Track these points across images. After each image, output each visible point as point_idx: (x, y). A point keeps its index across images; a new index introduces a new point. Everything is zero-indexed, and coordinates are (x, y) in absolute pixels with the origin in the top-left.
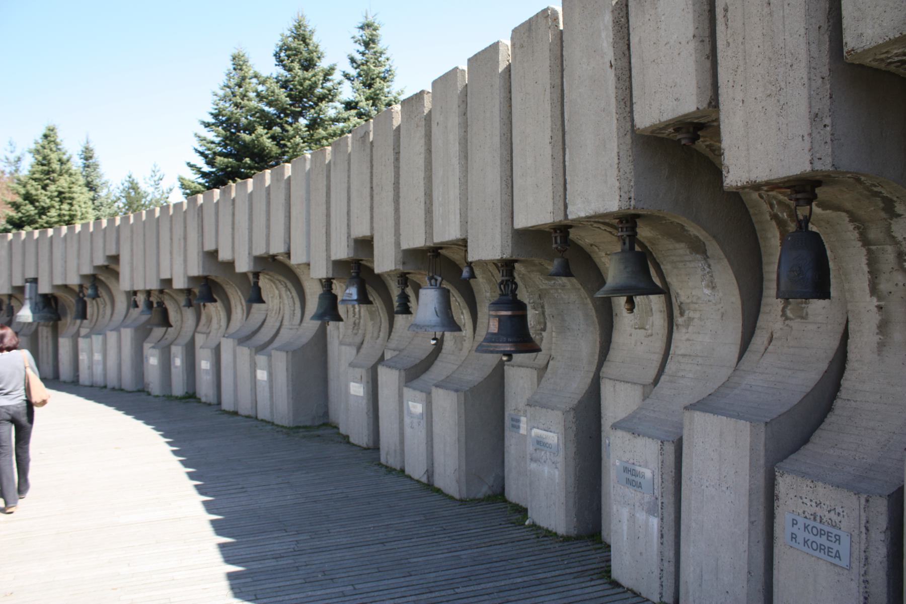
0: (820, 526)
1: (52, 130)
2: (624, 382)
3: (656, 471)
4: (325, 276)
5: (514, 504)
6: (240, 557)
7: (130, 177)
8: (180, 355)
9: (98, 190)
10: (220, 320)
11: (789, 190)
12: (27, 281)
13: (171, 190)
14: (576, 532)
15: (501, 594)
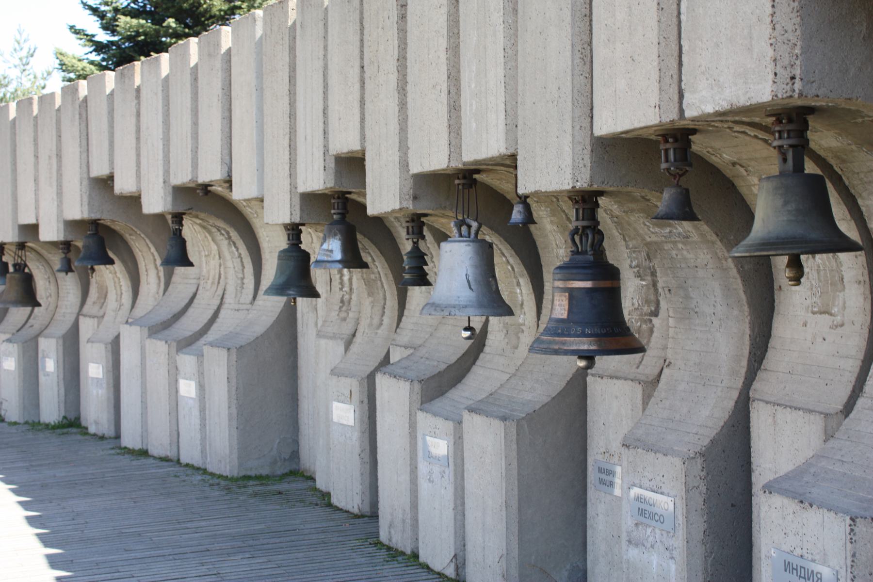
2: (791, 407)
3: (843, 572)
8: (53, 354)
10: (122, 294)
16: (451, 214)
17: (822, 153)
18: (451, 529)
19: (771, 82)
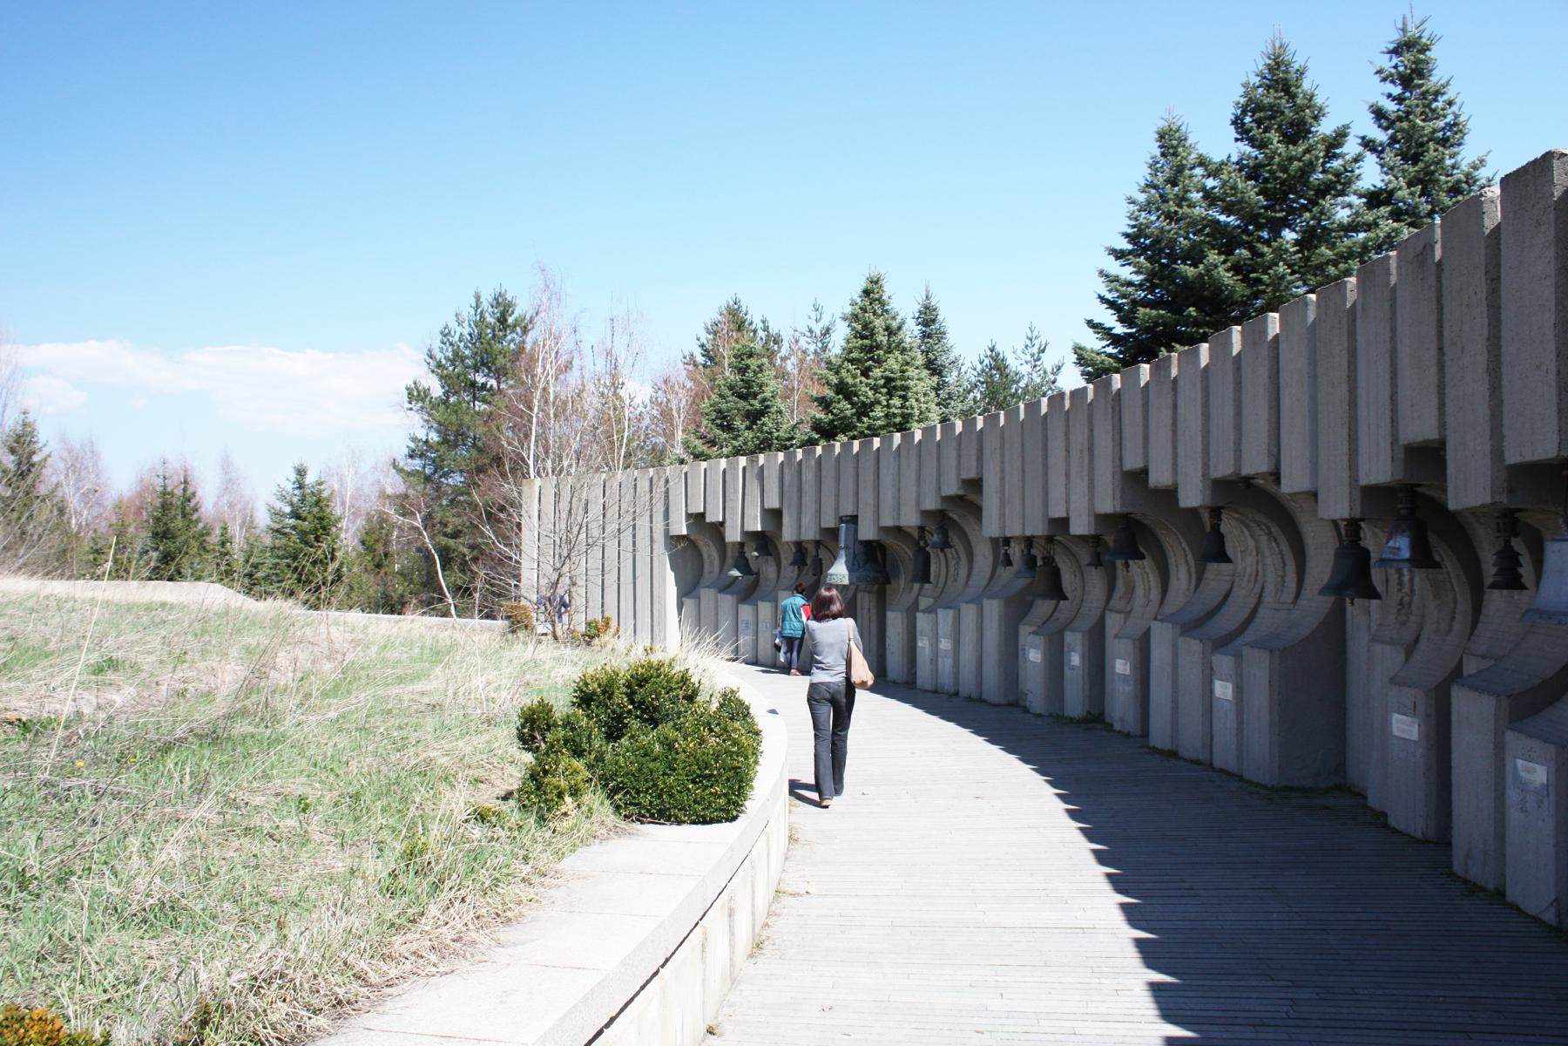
1: (876, 282)
4: (1346, 515)
6: (1189, 1013)
7: (992, 351)
8: (1079, 648)
9: (944, 373)
10: (1150, 589)
12: (841, 520)
13: (1059, 368)
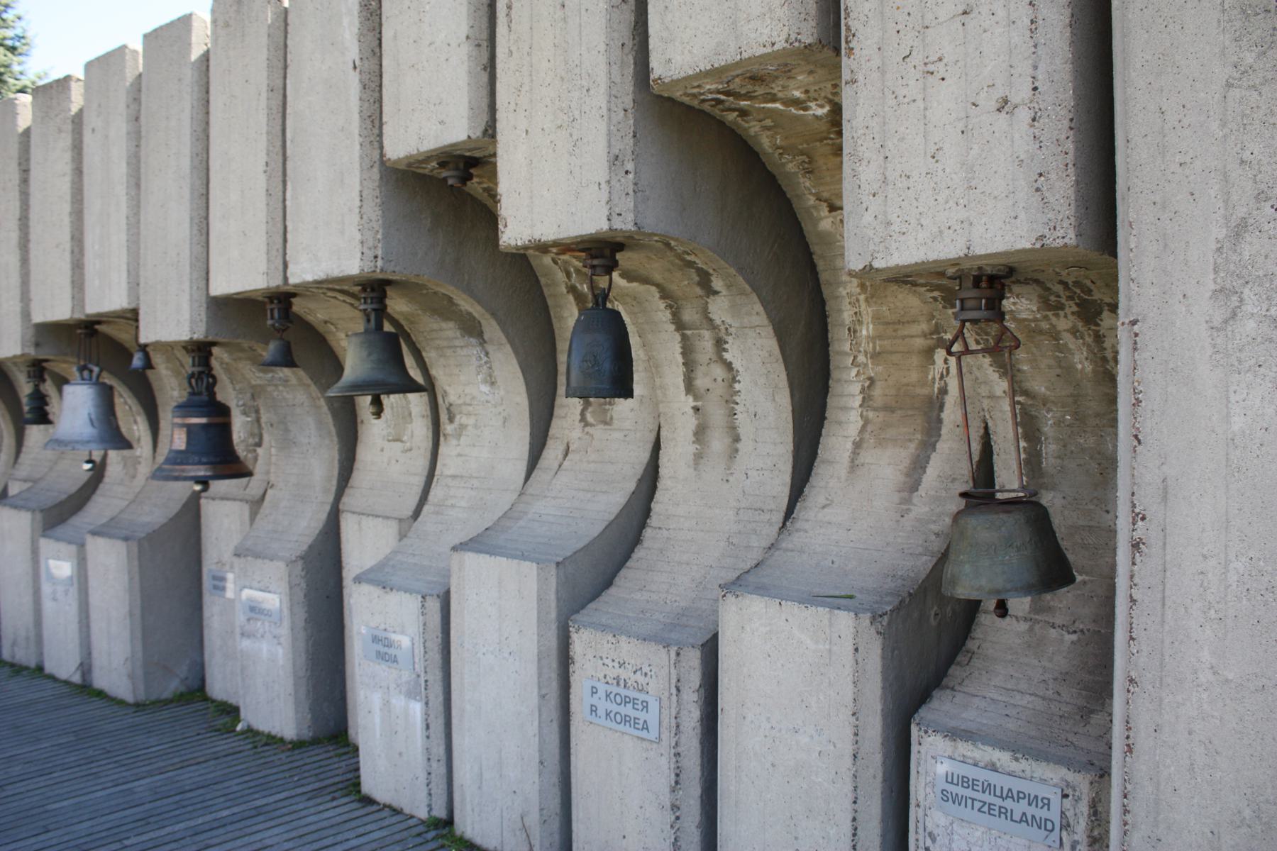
0: (624, 692)
2: (373, 515)
3: (417, 638)
5: (219, 702)
11: (584, 254)
14: (311, 734)
15: (197, 838)
16: (75, 360)
17: (396, 316)
18: (77, 641)
19: (359, 260)
